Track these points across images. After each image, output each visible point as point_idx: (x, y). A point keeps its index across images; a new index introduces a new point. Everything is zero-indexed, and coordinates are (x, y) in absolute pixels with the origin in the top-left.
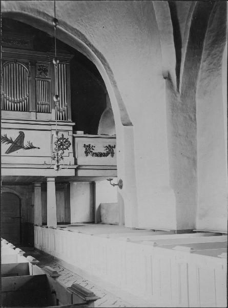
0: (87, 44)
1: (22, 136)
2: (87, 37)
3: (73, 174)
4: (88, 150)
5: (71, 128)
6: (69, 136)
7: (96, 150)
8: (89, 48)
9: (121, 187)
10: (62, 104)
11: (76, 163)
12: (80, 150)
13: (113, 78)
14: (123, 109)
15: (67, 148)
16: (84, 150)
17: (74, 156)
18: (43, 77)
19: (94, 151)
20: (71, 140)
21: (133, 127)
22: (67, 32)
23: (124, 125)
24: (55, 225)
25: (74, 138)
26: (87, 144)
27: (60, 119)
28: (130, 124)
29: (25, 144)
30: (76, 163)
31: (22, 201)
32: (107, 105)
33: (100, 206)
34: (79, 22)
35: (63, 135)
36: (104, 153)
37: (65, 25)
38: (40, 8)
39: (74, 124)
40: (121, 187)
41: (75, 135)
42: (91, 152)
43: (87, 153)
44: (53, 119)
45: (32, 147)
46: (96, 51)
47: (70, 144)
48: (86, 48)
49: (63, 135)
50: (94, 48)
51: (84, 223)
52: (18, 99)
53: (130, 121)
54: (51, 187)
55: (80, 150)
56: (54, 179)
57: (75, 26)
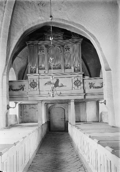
0: (85, 31)
1: (58, 81)
2: (85, 27)
3: (83, 98)
4: (91, 86)
5: (82, 75)
6: (81, 78)
7: (96, 85)
8: (87, 33)
9: (105, 104)
10: (78, 63)
11: (84, 92)
12: (87, 85)
13: (100, 46)
14: (105, 61)
15: (80, 85)
16: (89, 85)
17: (112, 86)
18: (68, 52)
19: (94, 86)
20: (82, 81)
21: (112, 71)
22: (74, 26)
23: (107, 71)
24: (75, 123)
25: (83, 80)
26: (90, 82)
27: (76, 71)
28: (110, 70)
29: (60, 84)
30: (84, 92)
31: (65, 111)
32: (17, 75)
33: (101, 113)
34: (80, 20)
35: (78, 79)
36: (100, 87)
37: (73, 23)
38: (33, 23)
39: (83, 73)
40: (105, 104)
41: (83, 78)
42: (93, 86)
43: (90, 87)
44: (73, 71)
45: (62, 86)
46: (90, 34)
47: (82, 83)
48: (86, 34)
49: (78, 79)
50: (89, 32)
51: (93, 122)
52: (56, 64)
53: (109, 68)
54: (72, 104)
55: (87, 85)
56: (73, 101)
57: (79, 23)
